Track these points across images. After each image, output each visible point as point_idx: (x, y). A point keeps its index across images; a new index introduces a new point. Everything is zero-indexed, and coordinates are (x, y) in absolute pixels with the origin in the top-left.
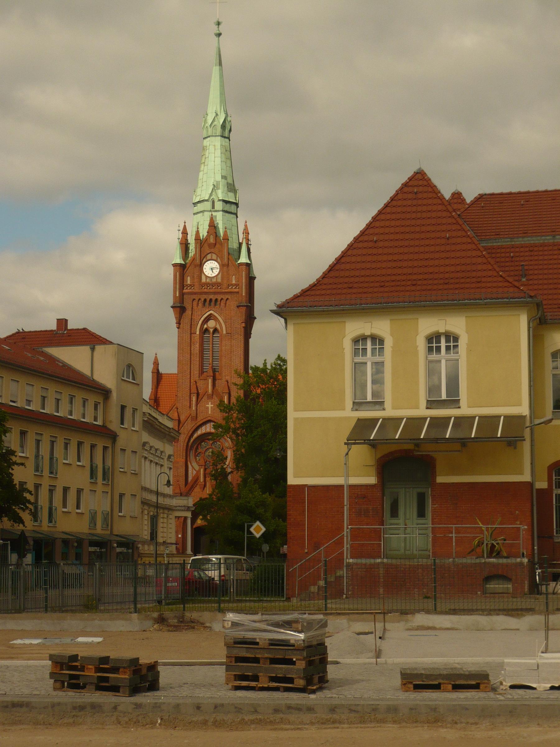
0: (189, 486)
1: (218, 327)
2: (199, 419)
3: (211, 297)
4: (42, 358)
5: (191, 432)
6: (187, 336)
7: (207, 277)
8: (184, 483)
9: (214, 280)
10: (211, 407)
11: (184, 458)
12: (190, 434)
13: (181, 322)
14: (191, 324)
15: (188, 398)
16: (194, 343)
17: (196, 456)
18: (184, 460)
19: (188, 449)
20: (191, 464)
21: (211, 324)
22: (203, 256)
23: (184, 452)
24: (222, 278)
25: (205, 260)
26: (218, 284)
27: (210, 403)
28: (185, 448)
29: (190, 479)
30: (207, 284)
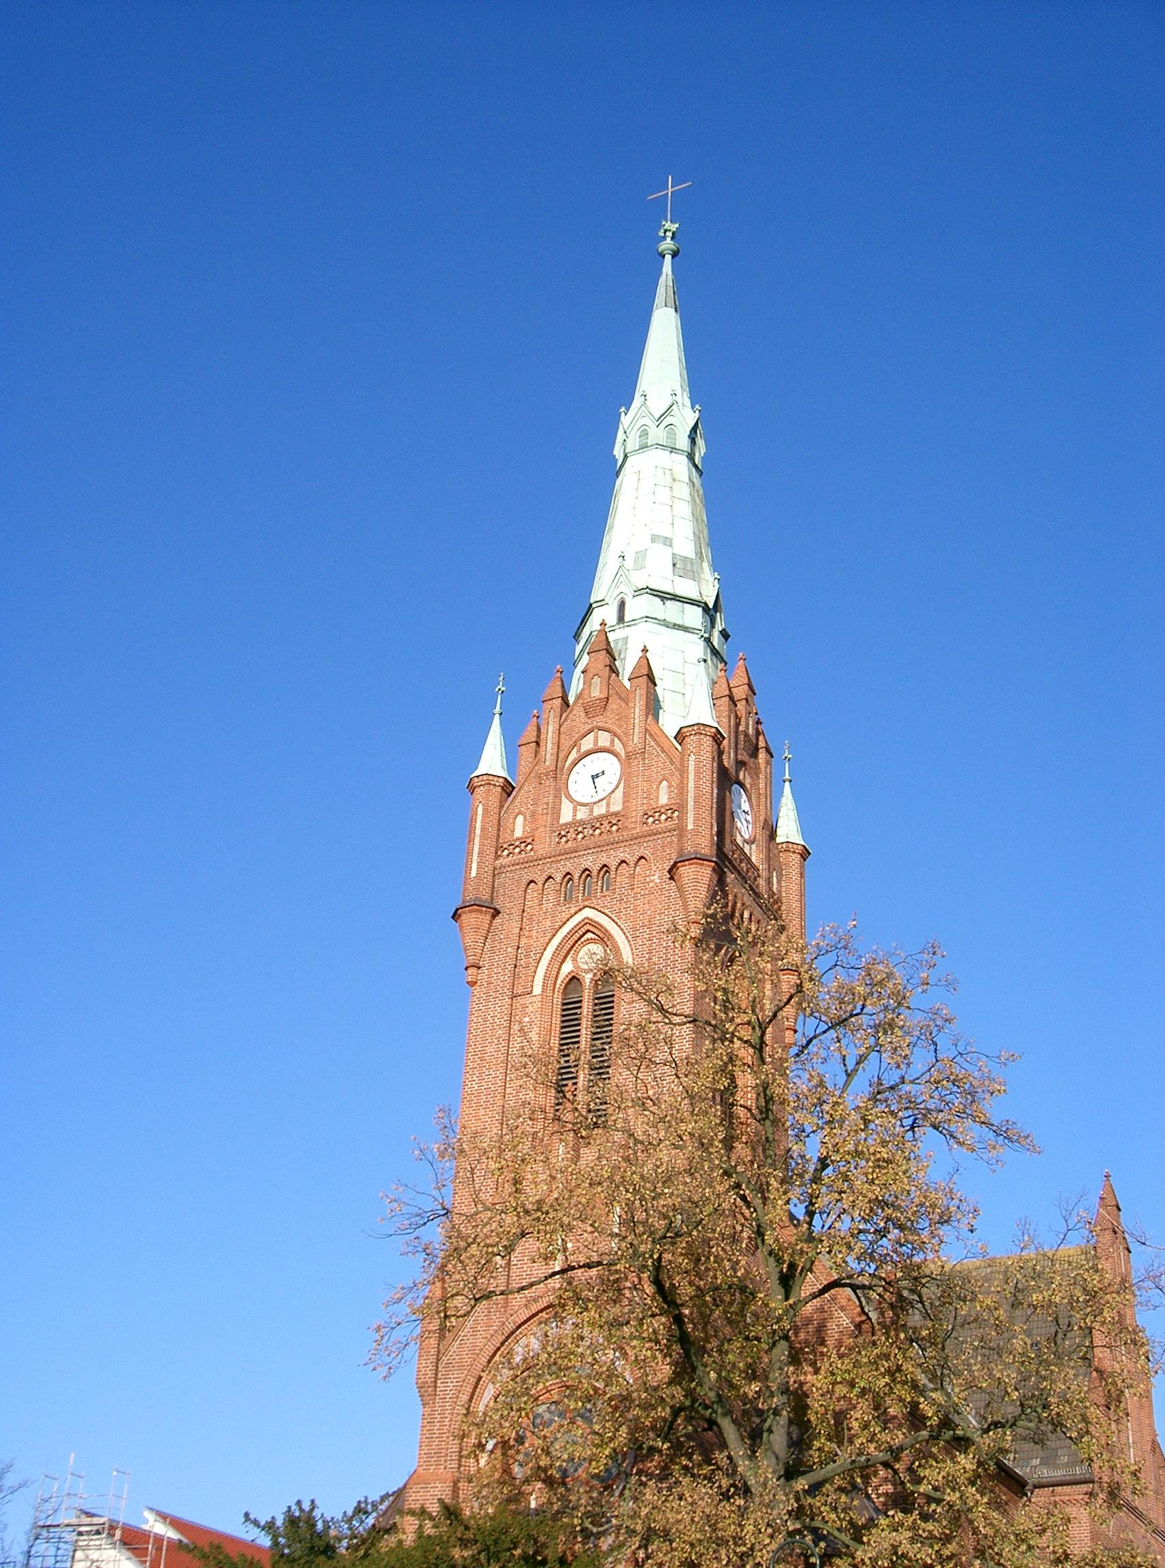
4: (859, 1480)
7: (577, 804)
9: (600, 810)
22: (566, 744)
25: (574, 755)
26: (614, 819)
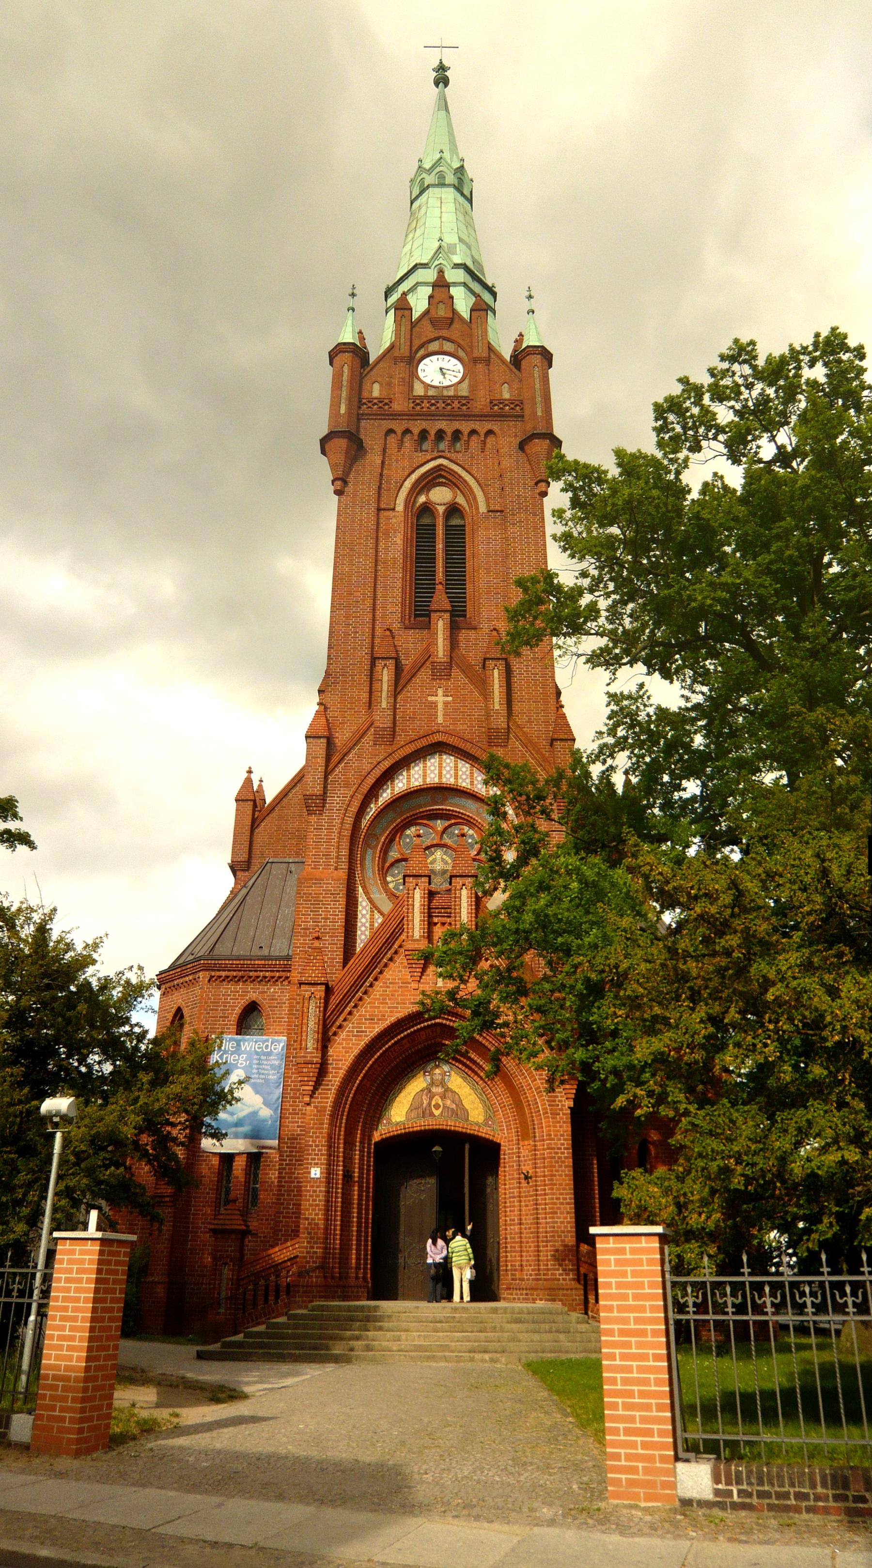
0: (357, 964)
1: (461, 500)
2: (401, 739)
3: (443, 425)
5: (371, 780)
6: (367, 514)
7: (427, 386)
8: (339, 957)
9: (451, 393)
11: (345, 866)
13: (351, 478)
14: (380, 488)
15: (365, 678)
16: (387, 534)
17: (384, 872)
18: (343, 874)
19: (356, 840)
20: (366, 893)
23: (345, 844)
24: (473, 388)
25: (422, 352)
27: (440, 692)
28: (347, 833)
29: (363, 935)
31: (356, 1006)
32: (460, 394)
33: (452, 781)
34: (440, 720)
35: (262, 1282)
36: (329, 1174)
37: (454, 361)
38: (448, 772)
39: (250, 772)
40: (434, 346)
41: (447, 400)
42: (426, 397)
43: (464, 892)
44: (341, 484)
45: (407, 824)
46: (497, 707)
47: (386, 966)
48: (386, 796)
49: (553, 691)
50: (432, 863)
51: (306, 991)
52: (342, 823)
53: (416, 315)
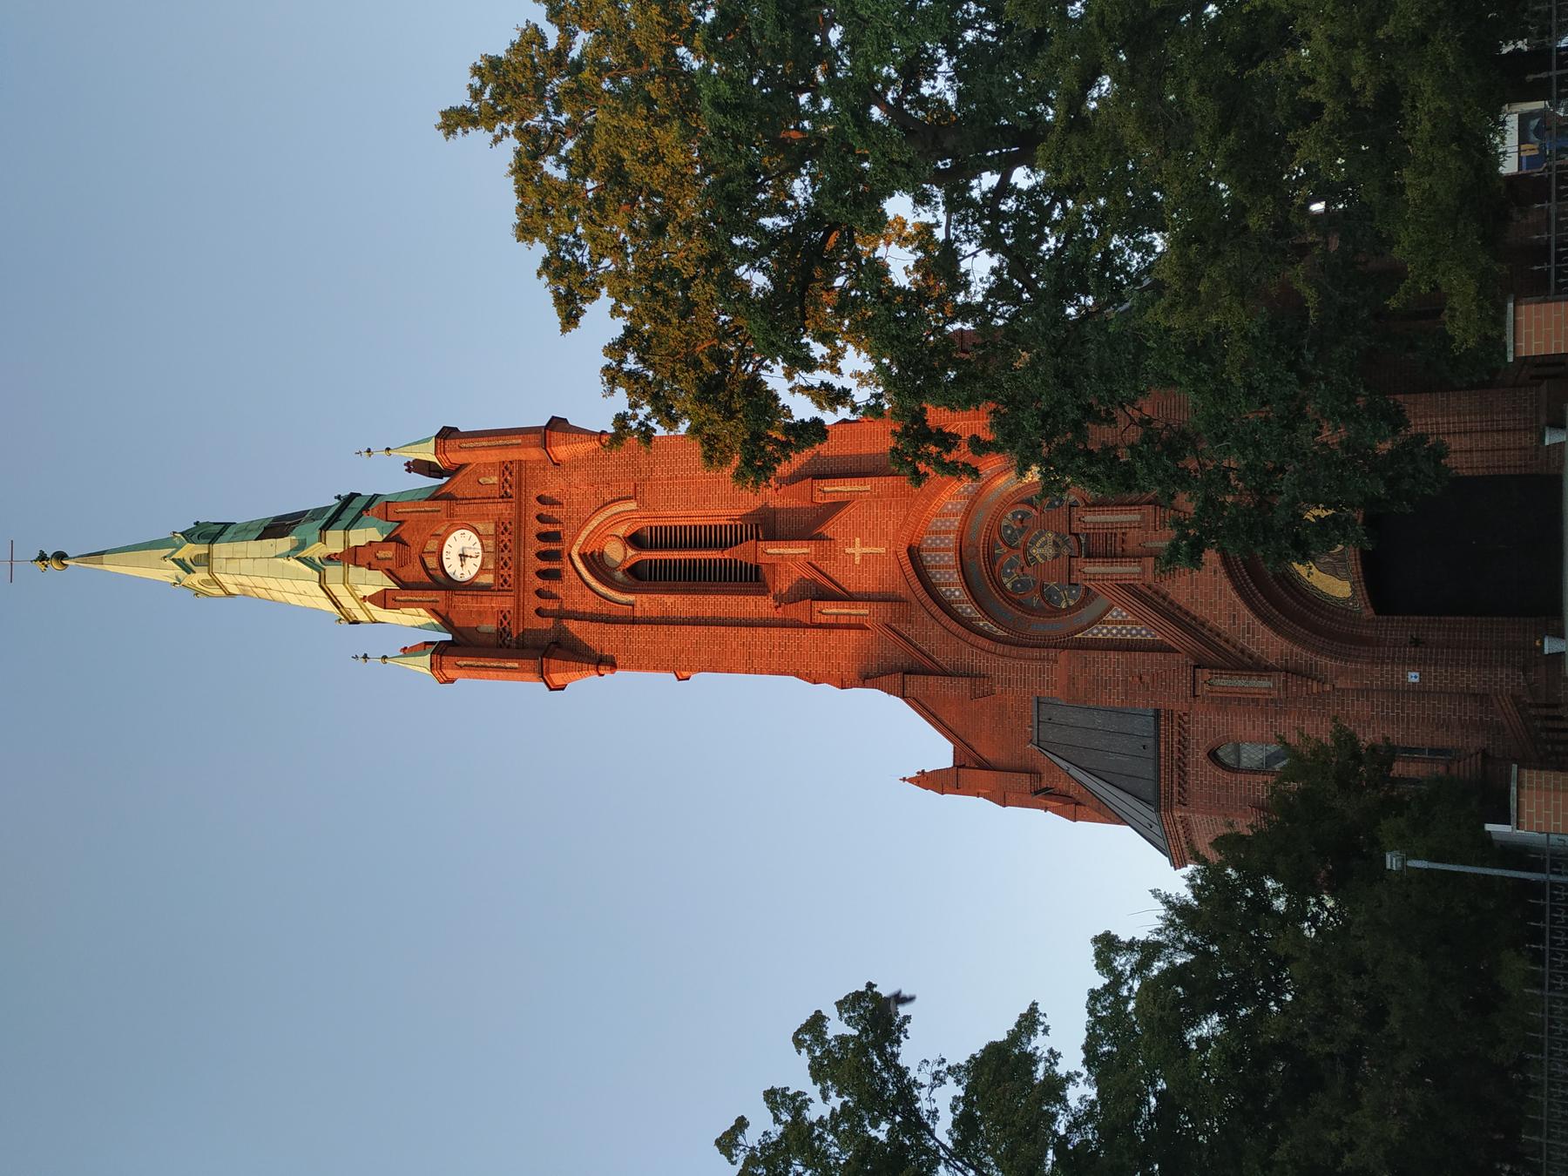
2: (902, 591)
3: (531, 553)
5: (954, 626)
7: (483, 569)
9: (491, 542)
10: (863, 545)
12: (961, 630)
21: (616, 552)
24: (483, 517)
27: (857, 560)
28: (1015, 651)
29: (1143, 633)
30: (501, 564)
31: (1218, 635)
32: (492, 531)
33: (952, 536)
34: (882, 550)
35: (1543, 735)
36: (1415, 663)
37: (450, 541)
38: (942, 541)
39: (926, 780)
40: (431, 562)
41: (501, 547)
42: (496, 572)
43: (1088, 518)
44: (603, 662)
45: (1002, 587)
46: (868, 487)
47: (1171, 603)
48: (969, 610)
49: (841, 427)
50: (1045, 558)
51: (1202, 689)
52: (1003, 656)
53: (391, 585)
